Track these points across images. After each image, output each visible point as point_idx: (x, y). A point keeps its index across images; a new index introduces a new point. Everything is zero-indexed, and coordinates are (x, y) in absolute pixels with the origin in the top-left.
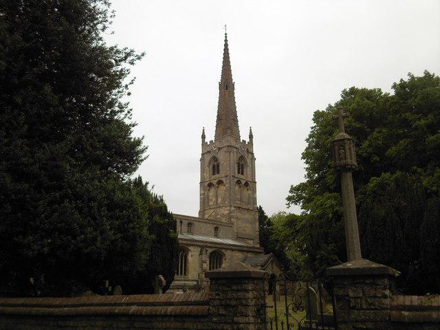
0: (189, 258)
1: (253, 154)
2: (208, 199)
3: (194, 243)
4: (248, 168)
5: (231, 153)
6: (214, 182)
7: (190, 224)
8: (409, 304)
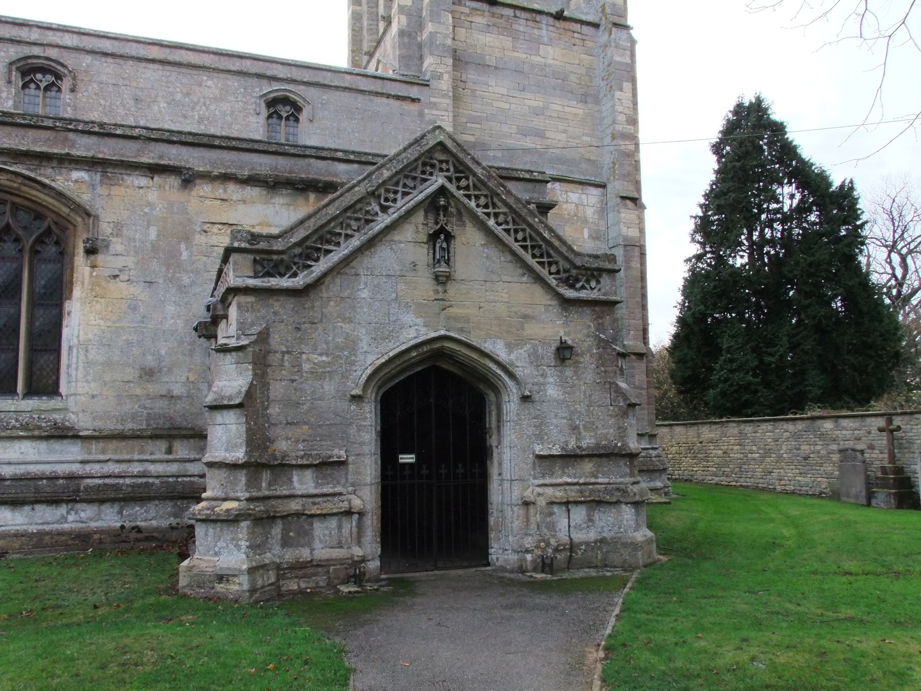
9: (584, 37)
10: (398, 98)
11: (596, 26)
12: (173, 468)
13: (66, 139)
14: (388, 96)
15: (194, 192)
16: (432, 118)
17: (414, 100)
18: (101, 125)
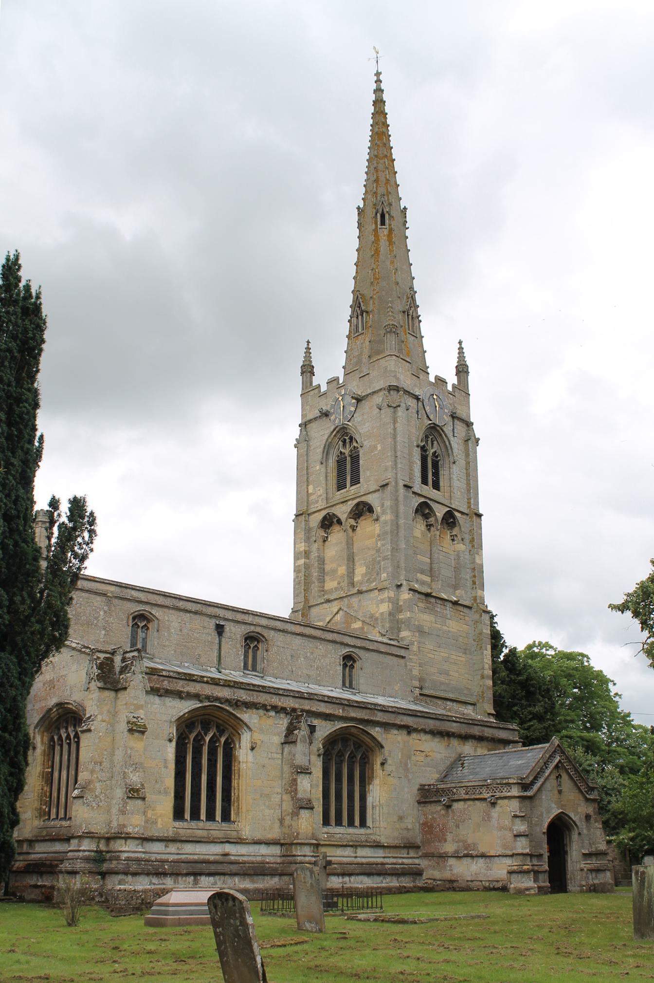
0: (243, 754)
1: (469, 424)
2: (322, 572)
3: (262, 698)
4: (455, 468)
5: (401, 412)
6: (342, 511)
7: (252, 640)
8: (209, 932)
9: (465, 615)
10: (397, 656)
11: (470, 608)
12: (410, 861)
13: (374, 713)
14: (393, 655)
15: (411, 737)
16: (411, 667)
17: (403, 657)
18: (384, 706)
